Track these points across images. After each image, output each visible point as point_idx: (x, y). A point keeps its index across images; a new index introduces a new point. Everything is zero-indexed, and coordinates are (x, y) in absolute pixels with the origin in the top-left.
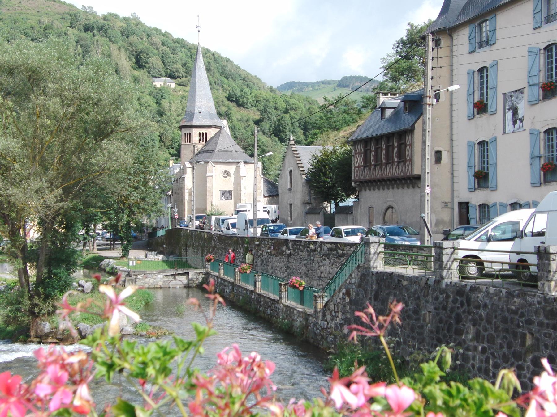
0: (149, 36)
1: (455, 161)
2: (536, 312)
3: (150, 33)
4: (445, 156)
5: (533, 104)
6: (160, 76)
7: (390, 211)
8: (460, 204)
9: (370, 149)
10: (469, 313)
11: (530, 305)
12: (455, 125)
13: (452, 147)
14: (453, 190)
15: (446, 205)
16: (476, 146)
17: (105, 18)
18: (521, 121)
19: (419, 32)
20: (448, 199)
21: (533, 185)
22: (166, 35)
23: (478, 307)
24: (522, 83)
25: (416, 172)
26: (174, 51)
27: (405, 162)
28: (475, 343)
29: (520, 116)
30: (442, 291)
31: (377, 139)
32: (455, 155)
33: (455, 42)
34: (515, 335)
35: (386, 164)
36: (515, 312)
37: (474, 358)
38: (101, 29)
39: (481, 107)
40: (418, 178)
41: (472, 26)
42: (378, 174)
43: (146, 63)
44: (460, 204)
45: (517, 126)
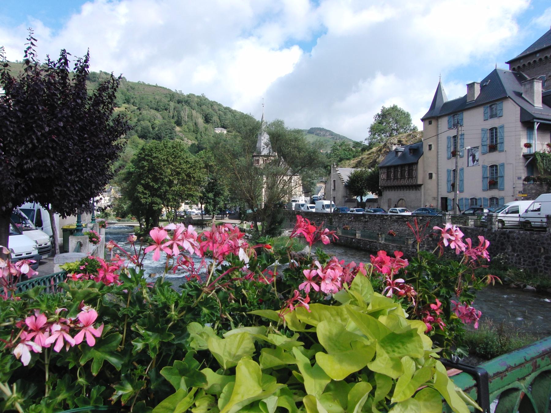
0: (212, 106)
1: (439, 178)
2: (546, 240)
3: (212, 104)
4: (434, 176)
5: (484, 154)
6: (218, 127)
7: (401, 201)
8: (442, 198)
9: (391, 172)
10: (509, 241)
11: (543, 237)
12: (439, 161)
13: (438, 171)
14: (438, 192)
15: (434, 198)
16: (452, 172)
17: (188, 96)
18: (477, 161)
19: (387, 111)
20: (436, 196)
21: (484, 190)
22: (219, 105)
23: (514, 239)
24: (478, 143)
25: (419, 182)
26: (225, 114)
27: (412, 178)
28: (513, 253)
29: (477, 159)
30: (492, 234)
31: (395, 167)
32: (439, 176)
33: (439, 123)
34: (535, 249)
35: (401, 179)
36: (535, 240)
37: (512, 259)
38: (186, 102)
39: (454, 154)
40: (420, 186)
41: (449, 116)
42: (396, 183)
43: (211, 120)
44: (442, 198)
45: (475, 163)
